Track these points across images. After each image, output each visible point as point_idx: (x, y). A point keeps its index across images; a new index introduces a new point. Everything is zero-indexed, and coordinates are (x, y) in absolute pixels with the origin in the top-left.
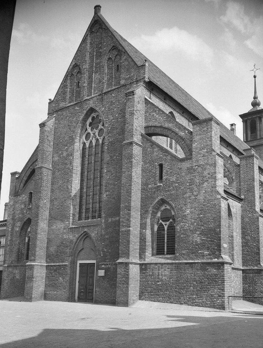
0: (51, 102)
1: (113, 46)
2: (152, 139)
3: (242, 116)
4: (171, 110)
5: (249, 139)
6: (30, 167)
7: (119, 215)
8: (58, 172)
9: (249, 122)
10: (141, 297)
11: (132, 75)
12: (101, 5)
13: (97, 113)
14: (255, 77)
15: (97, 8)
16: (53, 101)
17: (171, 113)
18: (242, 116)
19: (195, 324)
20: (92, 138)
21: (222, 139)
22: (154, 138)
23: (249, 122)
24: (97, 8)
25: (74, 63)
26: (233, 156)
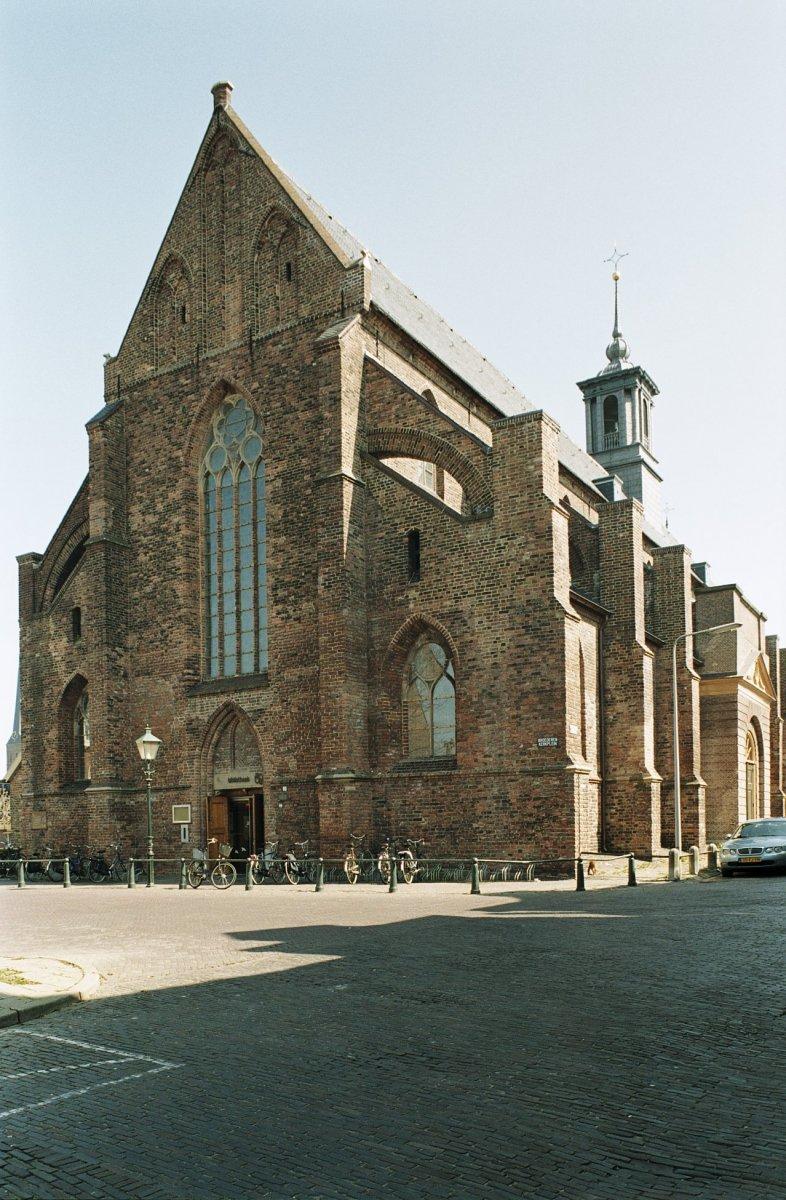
0: (110, 363)
1: (273, 209)
2: (445, 503)
3: (583, 386)
4: (428, 385)
5: (600, 448)
6: (68, 539)
7: (314, 660)
8: (146, 554)
9: (600, 400)
10: (136, 882)
11: (327, 292)
12: (223, 81)
13: (238, 396)
14: (616, 279)
15: (220, 91)
16: (116, 359)
17: (428, 393)
18: (583, 386)
19: (335, 957)
20: (230, 462)
21: (563, 470)
22: (388, 462)
23: (600, 400)
24: (220, 91)
25: (166, 255)
26: (571, 496)
